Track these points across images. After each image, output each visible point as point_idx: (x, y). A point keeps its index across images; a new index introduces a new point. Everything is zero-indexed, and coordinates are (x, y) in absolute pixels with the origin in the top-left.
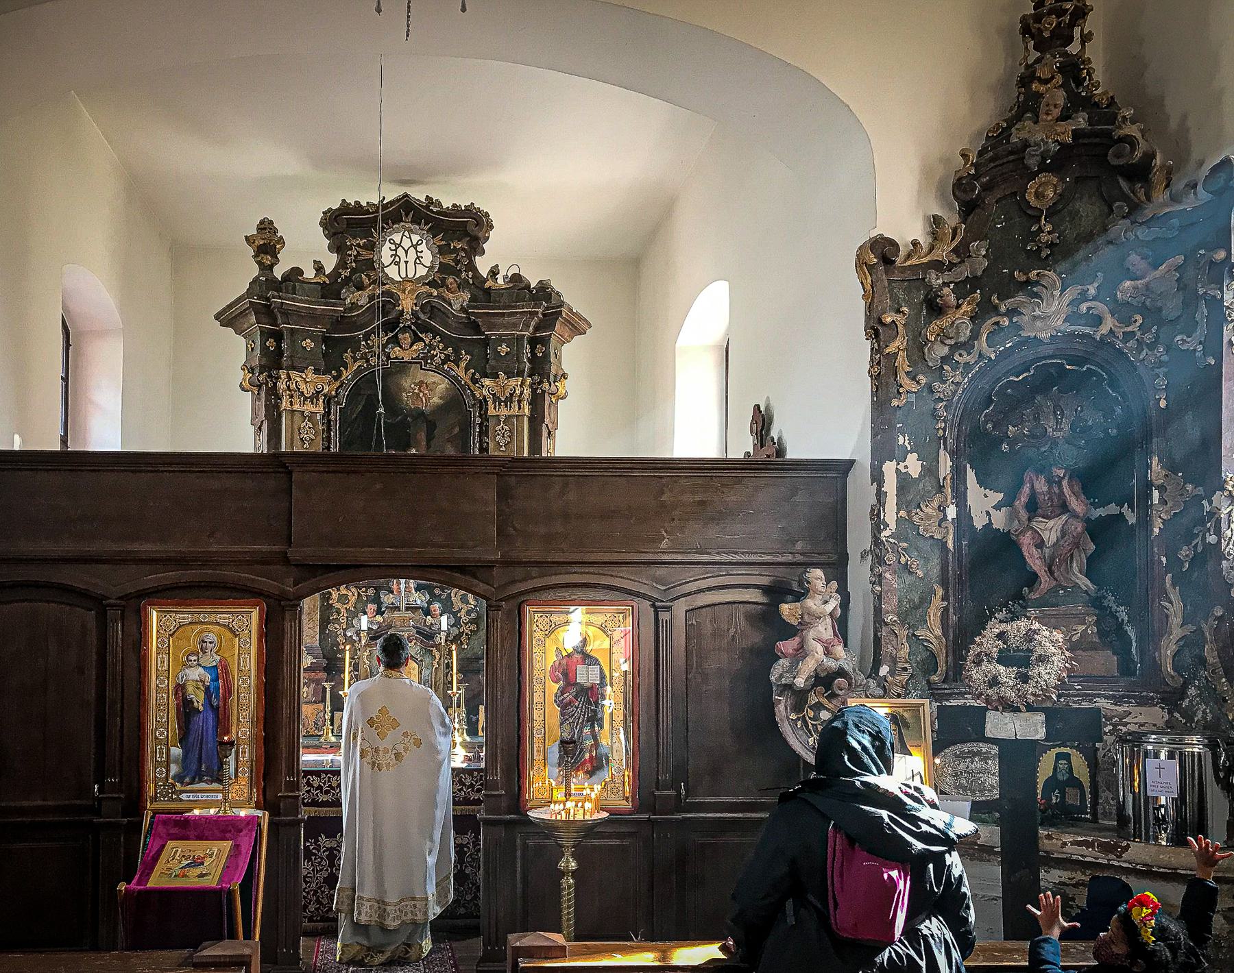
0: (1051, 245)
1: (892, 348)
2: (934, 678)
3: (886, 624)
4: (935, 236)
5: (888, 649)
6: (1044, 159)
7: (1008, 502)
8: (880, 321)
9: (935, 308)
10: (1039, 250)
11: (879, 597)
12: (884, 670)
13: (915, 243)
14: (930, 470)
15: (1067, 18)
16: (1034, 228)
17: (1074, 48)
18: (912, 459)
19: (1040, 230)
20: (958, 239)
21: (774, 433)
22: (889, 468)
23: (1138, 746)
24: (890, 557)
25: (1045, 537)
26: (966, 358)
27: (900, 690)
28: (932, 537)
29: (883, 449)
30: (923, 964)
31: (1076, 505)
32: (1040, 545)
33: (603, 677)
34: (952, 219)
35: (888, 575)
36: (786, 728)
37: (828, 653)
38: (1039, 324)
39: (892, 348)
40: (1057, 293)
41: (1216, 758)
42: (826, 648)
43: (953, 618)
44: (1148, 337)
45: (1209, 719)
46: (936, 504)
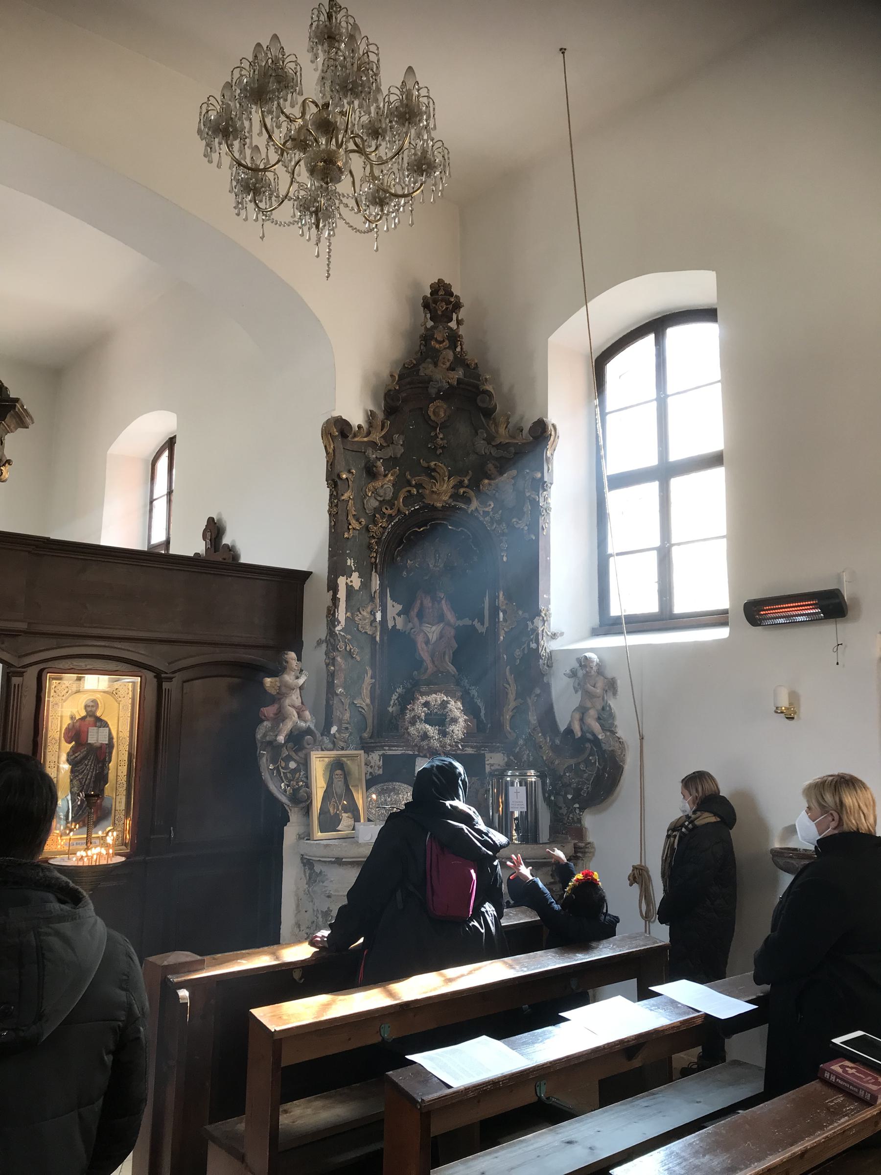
0: (443, 448)
1: (345, 497)
2: (366, 735)
3: (337, 695)
4: (370, 424)
5: (337, 713)
6: (439, 391)
7: (405, 612)
8: (339, 476)
9: (371, 473)
10: (436, 449)
11: (332, 675)
12: (334, 730)
13: (360, 427)
14: (366, 585)
15: (451, 307)
16: (433, 434)
17: (453, 325)
18: (355, 575)
19: (436, 436)
20: (385, 430)
21: (226, 540)
22: (342, 581)
23: (502, 779)
24: (341, 646)
25: (430, 637)
26: (389, 512)
27: (342, 744)
28: (366, 633)
29: (336, 568)
30: (483, 931)
31: (450, 616)
32: (427, 642)
33: (111, 738)
34: (380, 416)
35: (339, 659)
36: (266, 776)
37: (300, 716)
38: (435, 496)
39: (345, 497)
40: (446, 478)
41: (544, 784)
42: (298, 713)
43: (378, 692)
44: (497, 516)
45: (531, 759)
46: (369, 610)
